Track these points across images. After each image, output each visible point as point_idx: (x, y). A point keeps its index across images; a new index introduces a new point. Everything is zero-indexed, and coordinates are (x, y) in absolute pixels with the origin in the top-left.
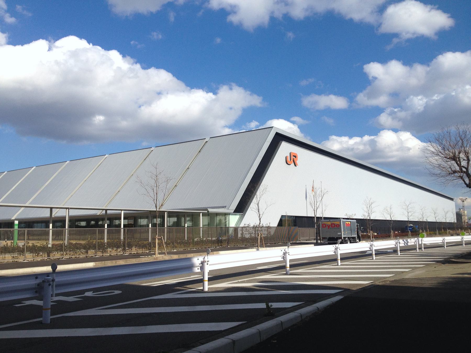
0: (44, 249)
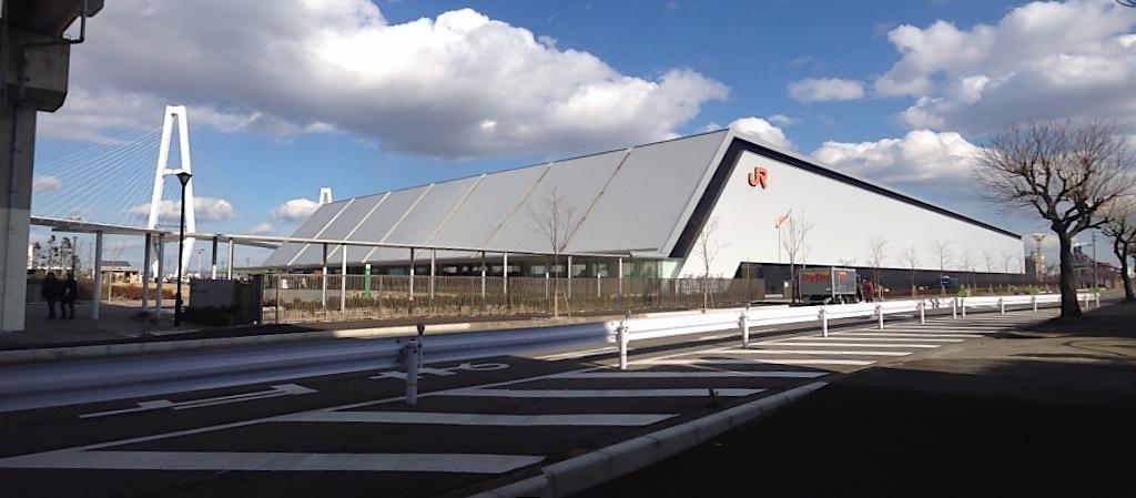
0: (404, 303)
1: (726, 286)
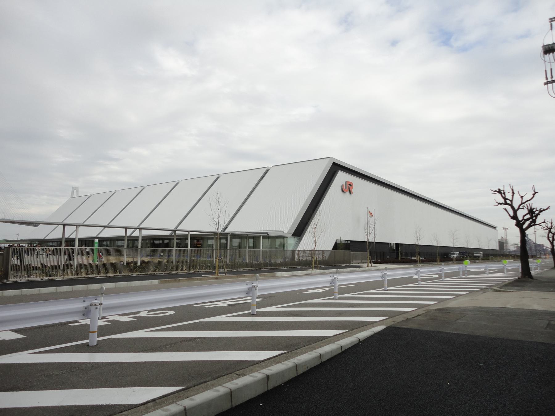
1: (327, 256)
